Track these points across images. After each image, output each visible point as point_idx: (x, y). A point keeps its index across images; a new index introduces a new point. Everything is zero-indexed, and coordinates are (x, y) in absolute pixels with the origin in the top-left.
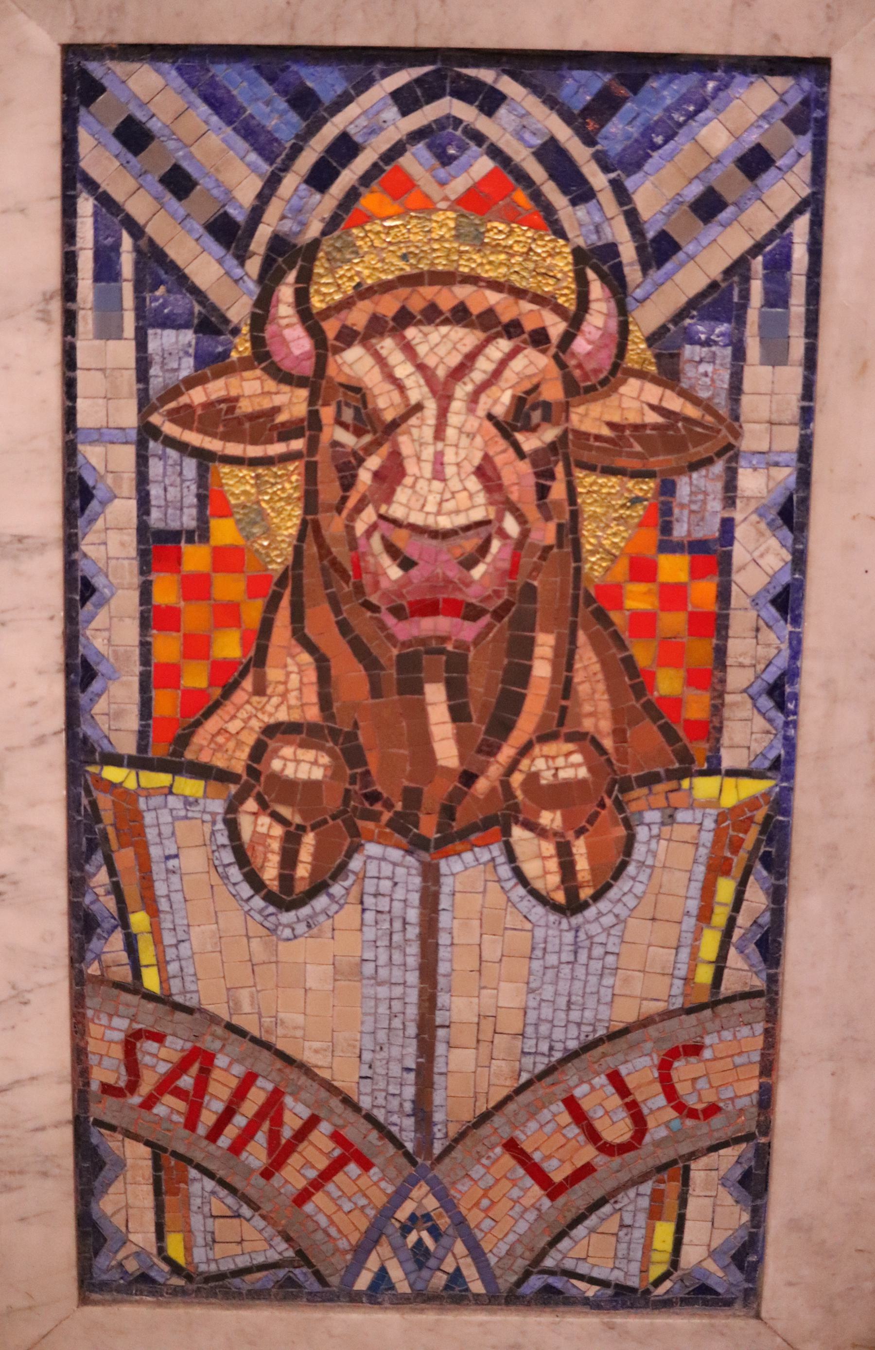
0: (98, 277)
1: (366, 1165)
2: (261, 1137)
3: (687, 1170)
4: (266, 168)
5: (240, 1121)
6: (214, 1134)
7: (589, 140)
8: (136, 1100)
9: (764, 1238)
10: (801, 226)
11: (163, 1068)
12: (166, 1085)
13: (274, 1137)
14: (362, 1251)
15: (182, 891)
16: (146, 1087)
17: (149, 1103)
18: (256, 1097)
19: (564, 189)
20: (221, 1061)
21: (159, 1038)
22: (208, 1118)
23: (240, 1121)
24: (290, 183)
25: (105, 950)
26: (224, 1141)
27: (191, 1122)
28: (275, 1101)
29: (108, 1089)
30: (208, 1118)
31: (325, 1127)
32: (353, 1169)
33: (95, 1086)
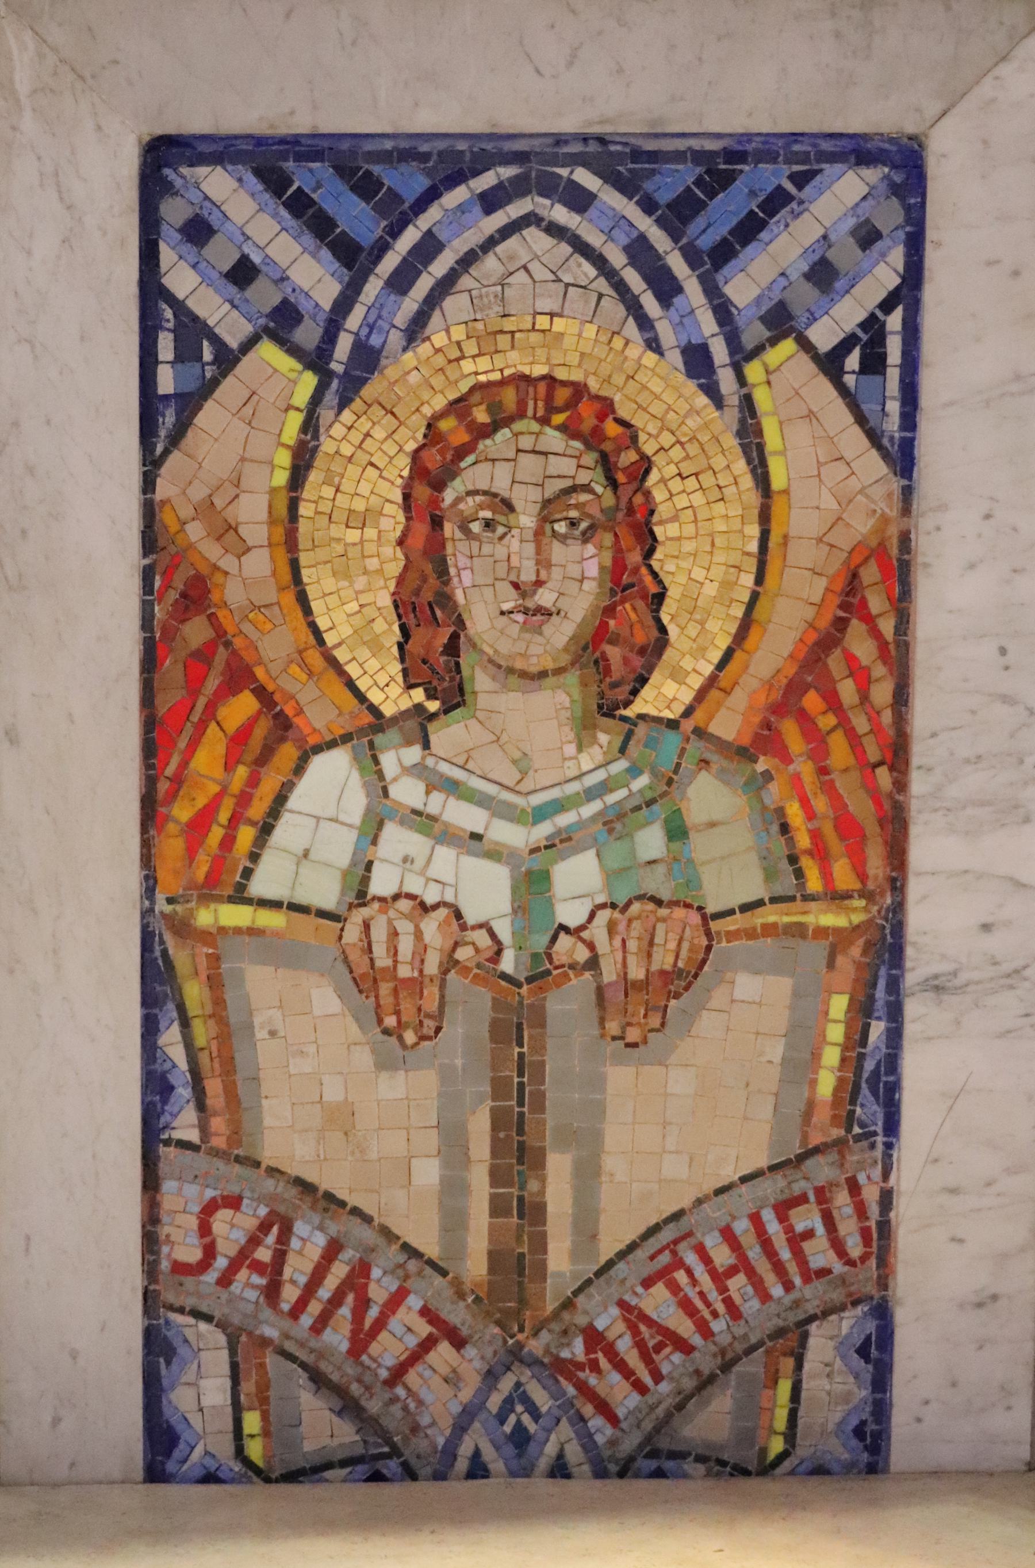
0: (642, 238)
1: (459, 1343)
2: (345, 1311)
3: (805, 1337)
4: (346, 274)
5: (325, 1293)
6: (296, 1311)
7: (675, 236)
8: (211, 1277)
9: (891, 1401)
10: (894, 321)
11: (240, 1237)
12: (241, 1259)
13: (363, 1303)
14: (460, 1428)
15: (184, 1211)
16: (221, 1263)
17: (225, 1281)
18: (339, 1271)
19: (871, 1235)
20: (300, 1228)
21: (234, 1202)
22: (290, 1294)
23: (325, 1293)
24: (373, 288)
25: (173, 1125)
26: (306, 1320)
27: (272, 1292)
28: (362, 1270)
29: (180, 1268)
30: (290, 1294)
31: (414, 1302)
32: (444, 1348)
33: (165, 1265)
